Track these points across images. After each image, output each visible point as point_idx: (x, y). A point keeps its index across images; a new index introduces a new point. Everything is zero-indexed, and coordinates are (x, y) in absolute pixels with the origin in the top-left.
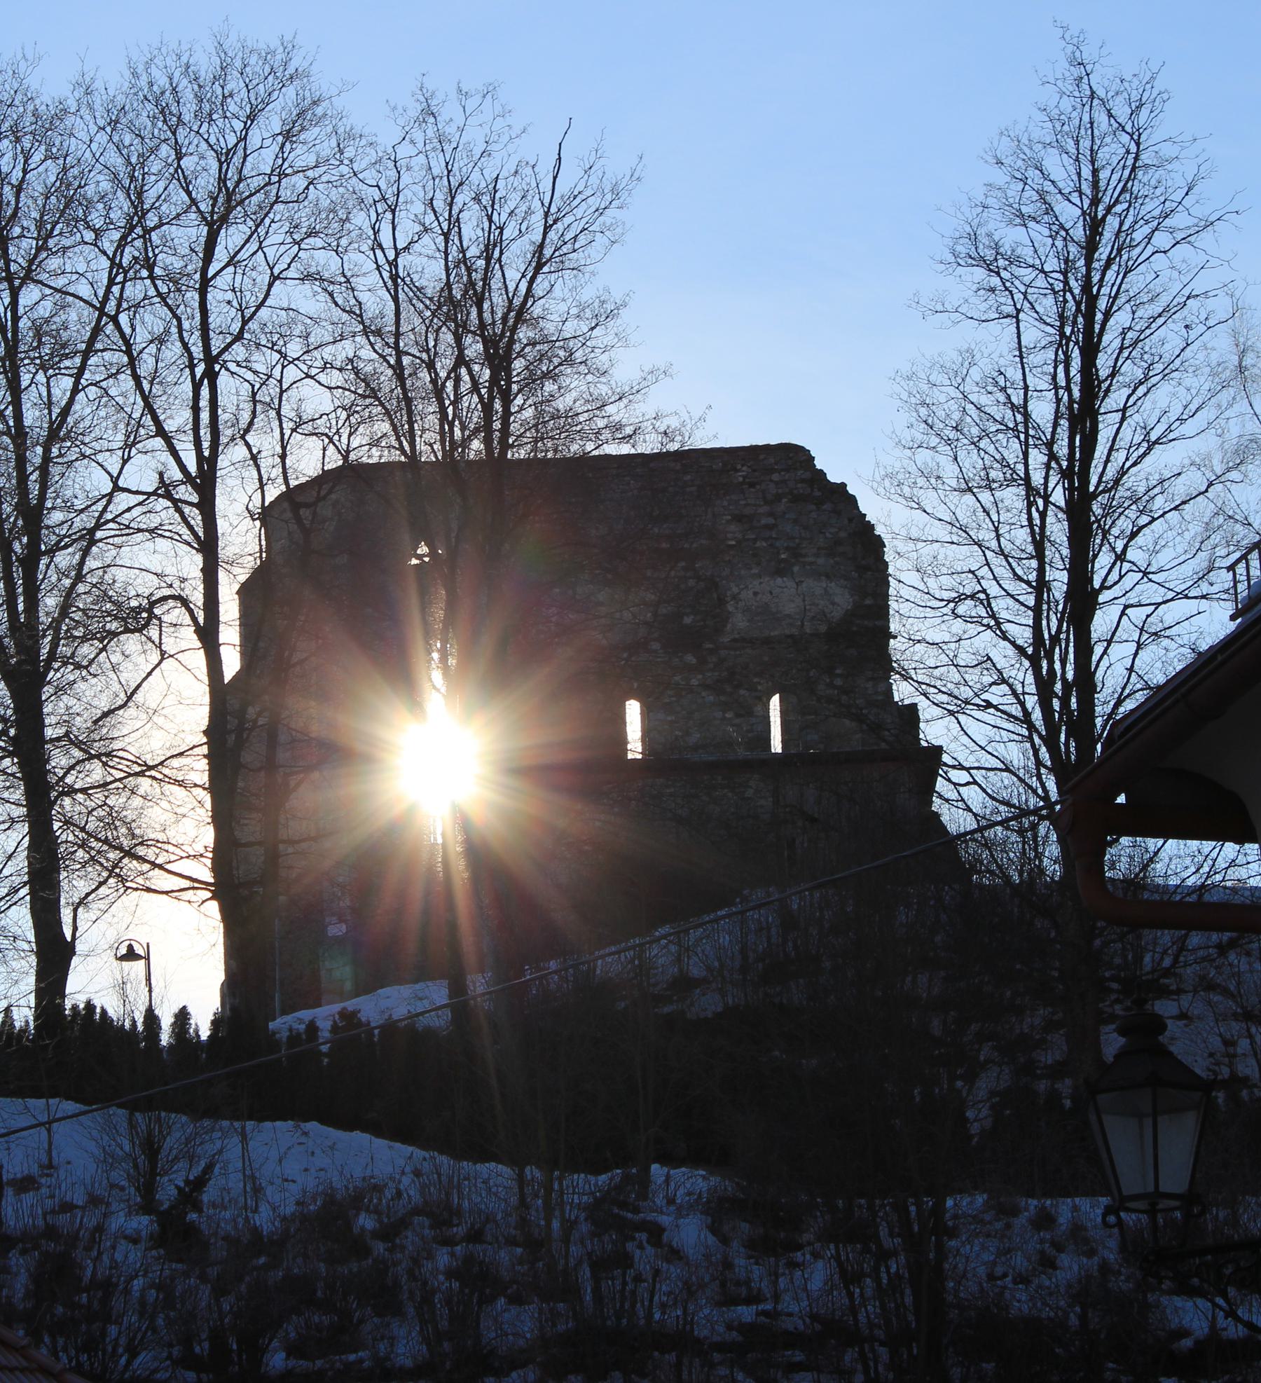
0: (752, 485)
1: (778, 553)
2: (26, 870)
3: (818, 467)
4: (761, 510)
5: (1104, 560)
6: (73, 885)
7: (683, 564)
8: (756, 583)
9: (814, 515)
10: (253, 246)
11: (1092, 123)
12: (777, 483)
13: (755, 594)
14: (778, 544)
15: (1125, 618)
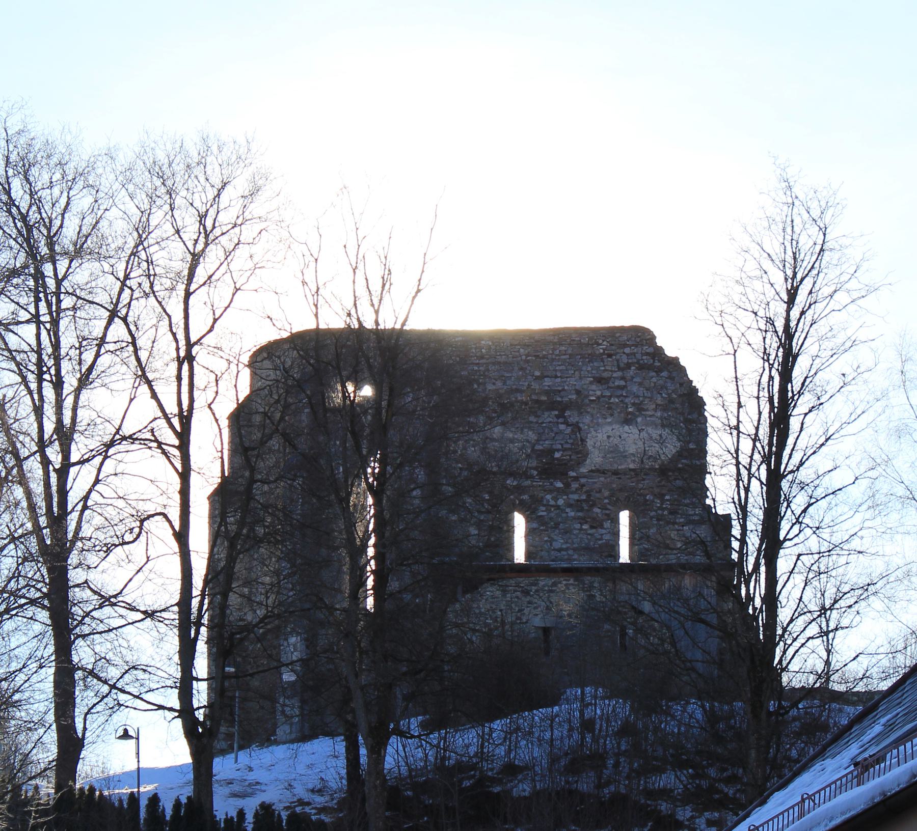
0: (610, 356)
1: (627, 407)
2: (53, 658)
3: (659, 344)
4: (615, 375)
5: (785, 526)
6: (84, 698)
7: (557, 413)
8: (610, 428)
9: (654, 380)
10: (224, 268)
11: (792, 221)
12: (628, 355)
13: (609, 437)
14: (627, 400)
15: (799, 562)
